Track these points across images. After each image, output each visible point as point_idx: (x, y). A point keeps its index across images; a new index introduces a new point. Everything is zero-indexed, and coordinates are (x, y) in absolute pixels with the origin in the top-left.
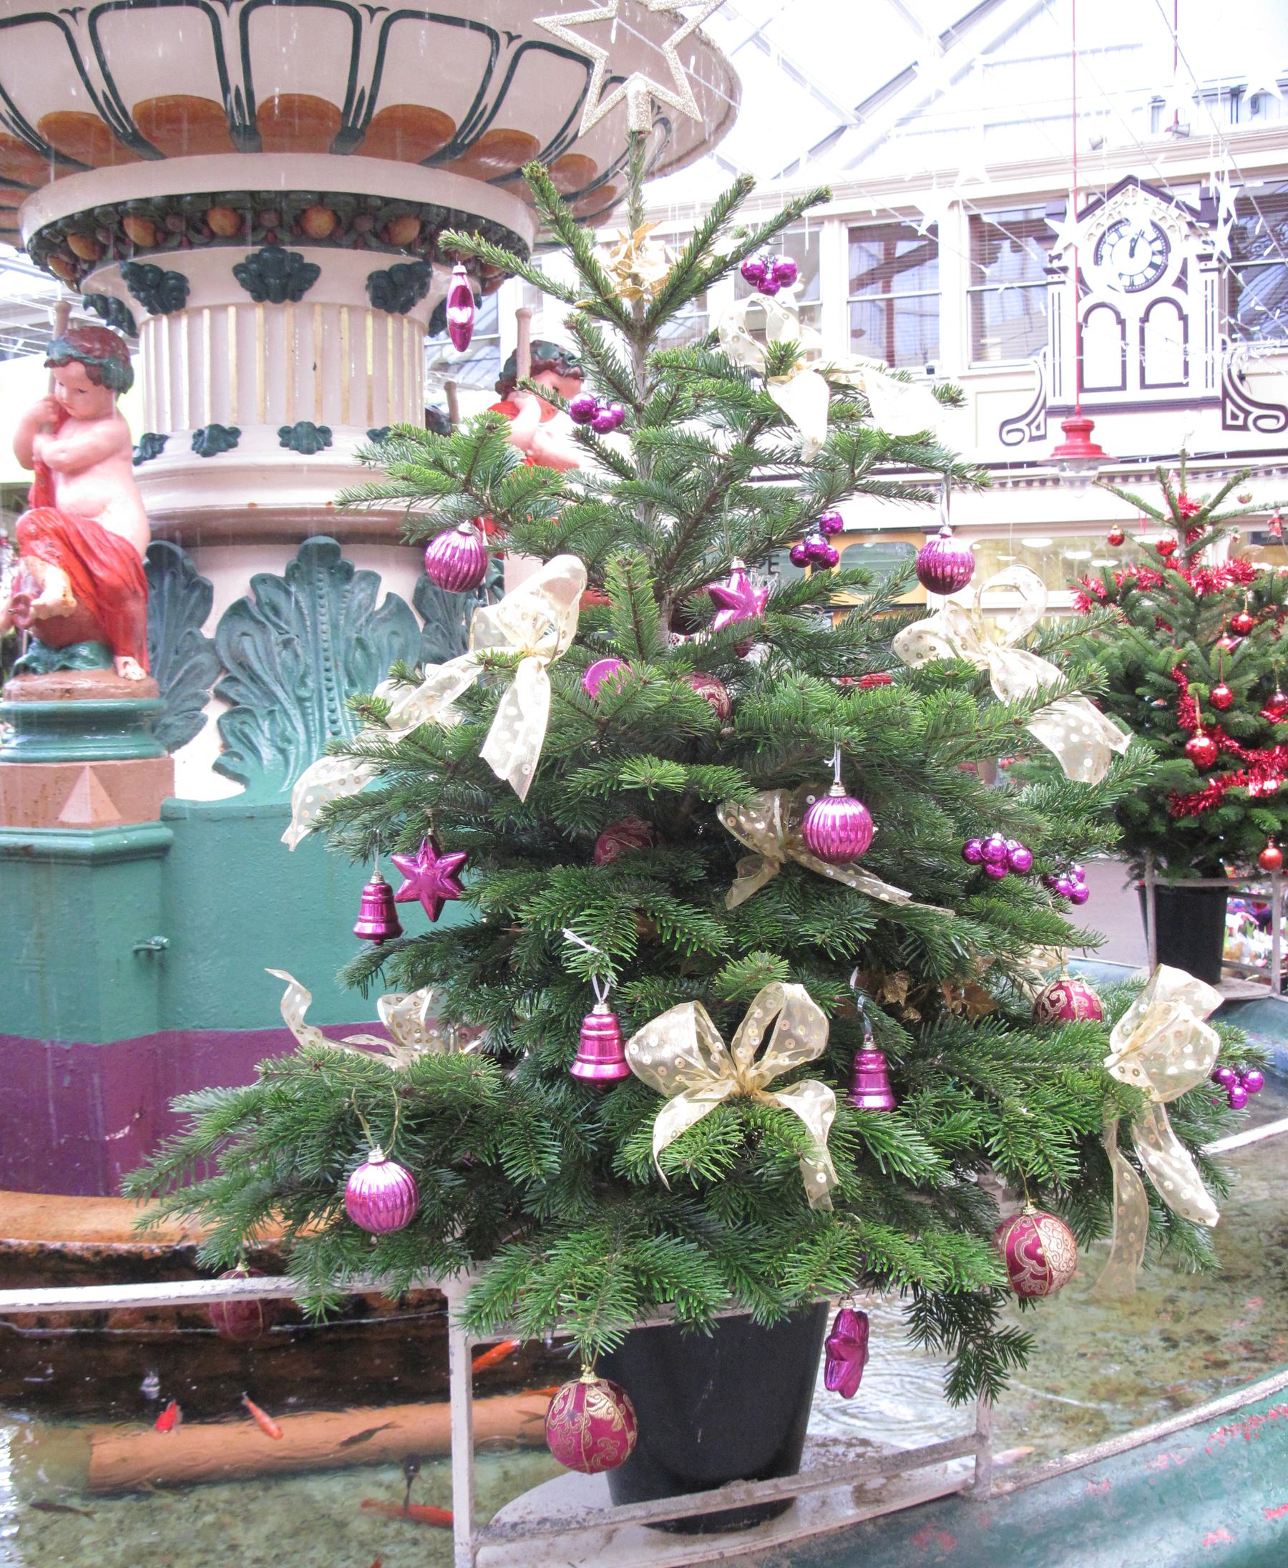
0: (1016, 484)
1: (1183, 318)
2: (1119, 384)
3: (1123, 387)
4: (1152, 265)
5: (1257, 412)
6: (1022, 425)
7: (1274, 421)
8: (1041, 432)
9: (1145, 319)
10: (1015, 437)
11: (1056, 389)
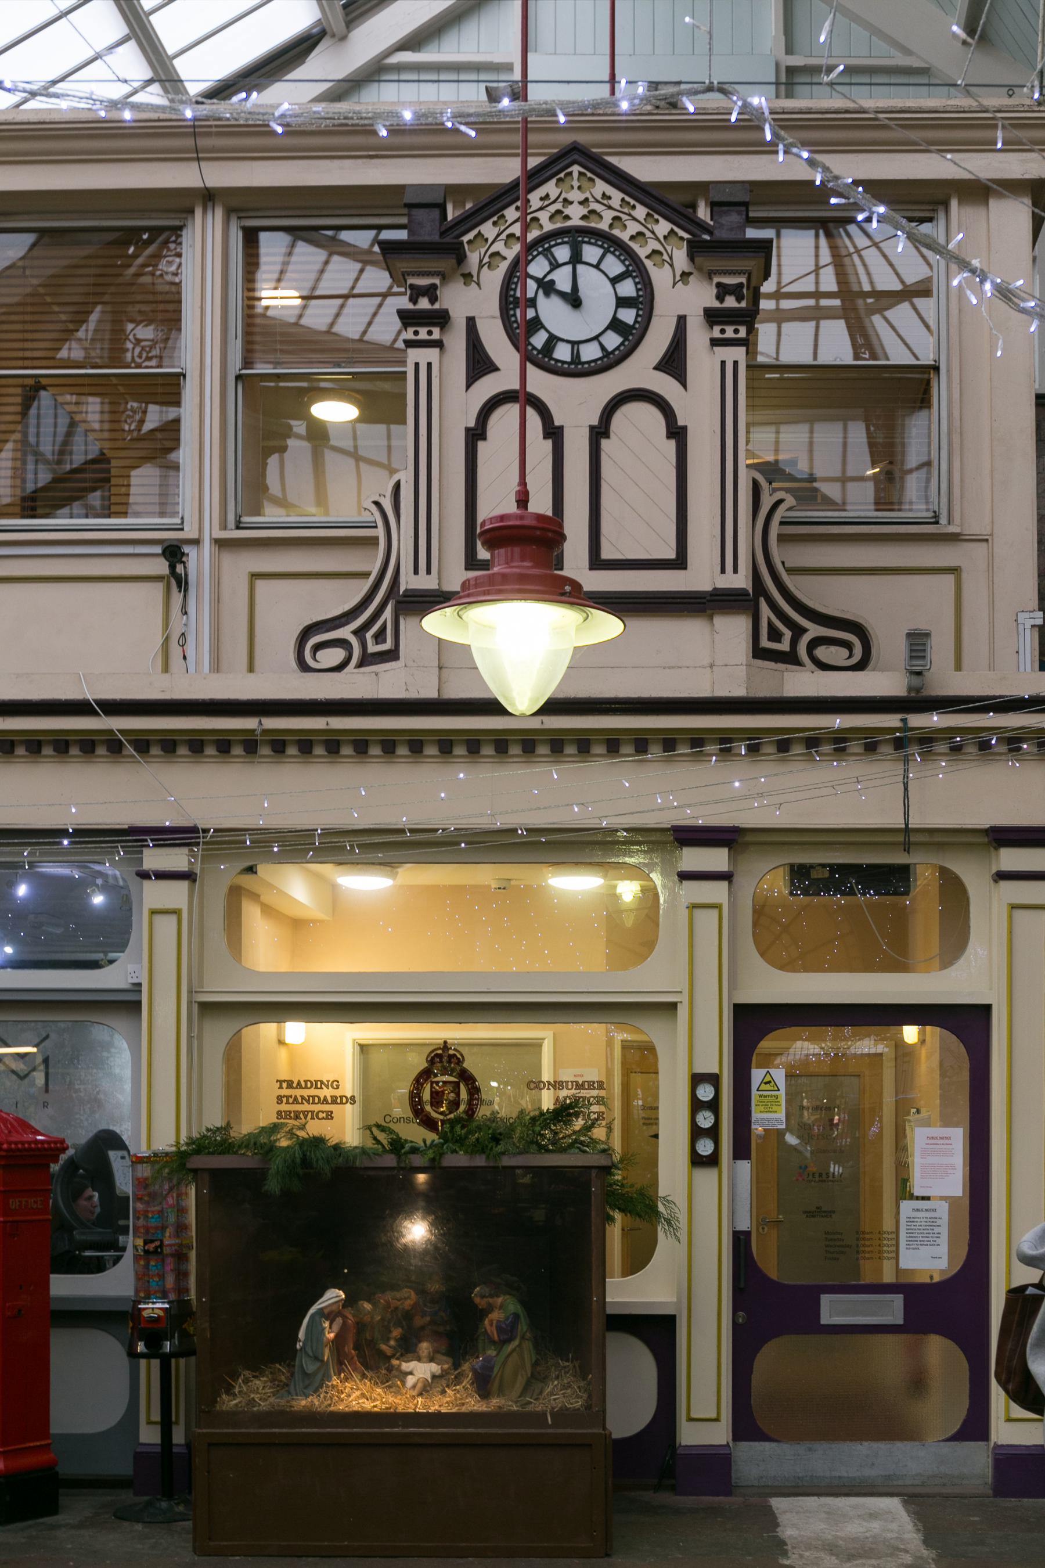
0: (783, 746)
1: (677, 433)
2: (670, 553)
3: (680, 562)
5: (814, 630)
6: (345, 633)
7: (844, 652)
9: (600, 432)
10: (335, 656)
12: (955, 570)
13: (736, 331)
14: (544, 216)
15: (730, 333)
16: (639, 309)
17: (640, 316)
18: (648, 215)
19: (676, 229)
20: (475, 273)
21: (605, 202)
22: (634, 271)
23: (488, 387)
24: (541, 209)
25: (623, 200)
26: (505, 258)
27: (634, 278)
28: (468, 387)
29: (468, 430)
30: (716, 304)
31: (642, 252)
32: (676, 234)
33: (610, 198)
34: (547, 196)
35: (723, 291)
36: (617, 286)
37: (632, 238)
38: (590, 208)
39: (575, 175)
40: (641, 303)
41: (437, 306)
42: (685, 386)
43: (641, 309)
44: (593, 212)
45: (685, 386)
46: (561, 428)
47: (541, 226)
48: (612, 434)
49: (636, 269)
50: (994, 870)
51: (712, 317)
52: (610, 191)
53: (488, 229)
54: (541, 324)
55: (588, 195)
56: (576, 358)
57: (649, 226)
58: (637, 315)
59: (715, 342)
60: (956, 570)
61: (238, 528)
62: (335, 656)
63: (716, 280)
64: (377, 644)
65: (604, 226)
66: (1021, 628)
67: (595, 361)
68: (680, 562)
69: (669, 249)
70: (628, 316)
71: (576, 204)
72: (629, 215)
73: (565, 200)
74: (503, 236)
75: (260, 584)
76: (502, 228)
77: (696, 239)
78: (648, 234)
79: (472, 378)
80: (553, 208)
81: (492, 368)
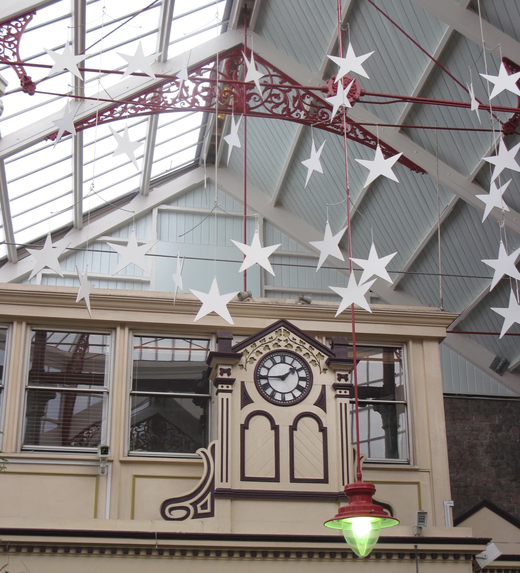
1: (323, 430)
3: (325, 480)
4: (299, 387)
6: (187, 504)
8: (208, 510)
9: (293, 428)
11: (225, 476)
12: (418, 483)
13: (345, 392)
14: (270, 345)
15: (343, 393)
16: (307, 382)
17: (308, 384)
18: (310, 347)
19: (321, 353)
20: (244, 365)
21: (294, 341)
22: (305, 367)
23: (249, 409)
24: (269, 342)
25: (300, 340)
26: (256, 360)
27: (305, 370)
28: (242, 408)
29: (241, 425)
30: (338, 382)
31: (308, 360)
32: (320, 354)
33: (295, 340)
34: (272, 337)
35: (340, 377)
36: (299, 372)
37: (304, 355)
38: (288, 343)
39: (282, 330)
40: (308, 379)
41: (230, 377)
42: (326, 412)
43: (308, 382)
44: (289, 344)
45: (326, 412)
46: (278, 426)
47: (269, 349)
48: (298, 429)
49: (306, 366)
50: (5, 571)
51: (336, 387)
52: (296, 337)
53: (249, 348)
54: (270, 385)
55: (287, 338)
56: (283, 399)
57: (310, 351)
58: (307, 384)
59: (337, 396)
60: (418, 483)
61: (128, 456)
62: (183, 513)
63: (337, 373)
64: (202, 509)
65: (293, 350)
66: (445, 507)
67: (291, 401)
68: (325, 480)
69: (318, 359)
70: (303, 384)
71: (283, 341)
72: (303, 346)
73: (279, 339)
74: (255, 351)
75: (138, 480)
76: (255, 348)
77: (331, 358)
78: (310, 354)
79: (243, 405)
80: (274, 342)
81: (251, 402)
